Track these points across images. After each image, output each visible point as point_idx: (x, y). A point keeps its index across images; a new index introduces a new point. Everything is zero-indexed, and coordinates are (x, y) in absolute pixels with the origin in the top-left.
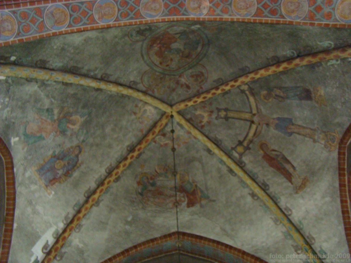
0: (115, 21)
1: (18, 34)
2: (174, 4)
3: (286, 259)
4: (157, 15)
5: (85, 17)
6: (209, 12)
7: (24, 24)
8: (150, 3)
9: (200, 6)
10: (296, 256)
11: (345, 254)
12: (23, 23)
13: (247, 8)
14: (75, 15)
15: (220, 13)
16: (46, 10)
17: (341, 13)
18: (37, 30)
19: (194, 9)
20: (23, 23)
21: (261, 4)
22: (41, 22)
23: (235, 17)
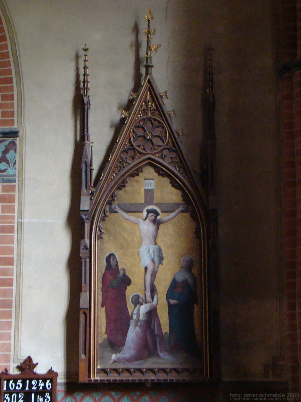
3: (245, 398)
10: (253, 395)
11: (292, 394)
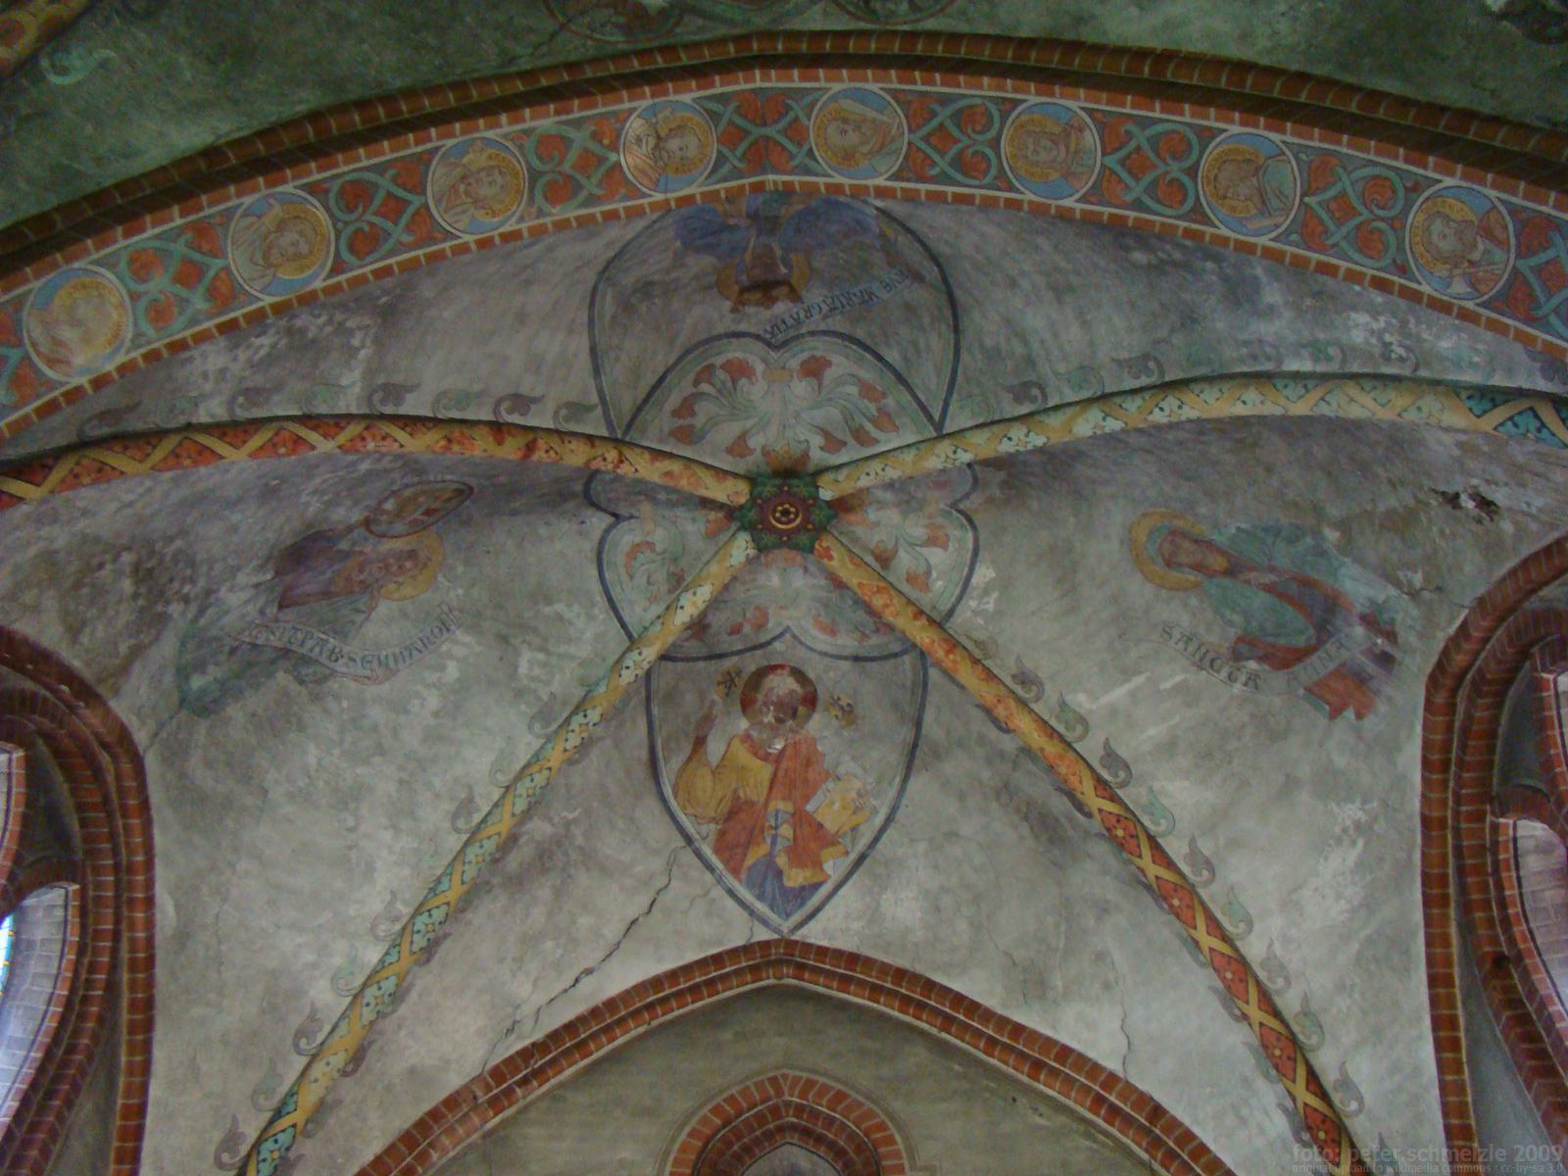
0: (1015, 103)
1: (1416, 188)
2: (767, 139)
4: (834, 98)
5: (1138, 149)
6: (619, 126)
7: (1381, 213)
8: (865, 149)
9: (657, 146)
12: (1383, 220)
13: (464, 178)
14: (1175, 169)
15: (571, 133)
16: (1283, 228)
17: (100, 296)
18: (1340, 171)
19: (680, 129)
20: (1383, 220)
21: (410, 210)
22: (1313, 194)
23: (507, 129)
